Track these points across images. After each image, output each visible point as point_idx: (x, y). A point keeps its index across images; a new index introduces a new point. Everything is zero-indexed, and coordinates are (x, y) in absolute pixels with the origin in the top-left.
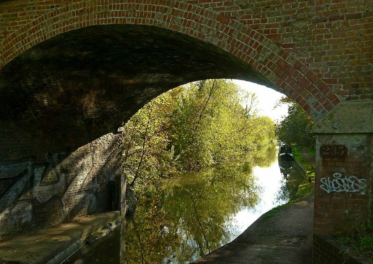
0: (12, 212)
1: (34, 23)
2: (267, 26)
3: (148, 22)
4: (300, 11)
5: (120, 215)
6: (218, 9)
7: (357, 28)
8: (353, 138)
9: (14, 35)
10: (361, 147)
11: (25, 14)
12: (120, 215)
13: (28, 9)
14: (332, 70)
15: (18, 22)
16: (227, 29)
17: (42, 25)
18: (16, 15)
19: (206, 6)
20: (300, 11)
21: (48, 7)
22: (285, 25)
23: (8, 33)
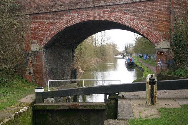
0: (49, 117)
1: (71, 18)
2: (143, 22)
3: (109, 19)
4: (151, 19)
5: (139, 104)
6: (130, 17)
7: (165, 23)
8: (165, 50)
9: (63, 22)
10: (167, 52)
11: (67, 15)
12: (139, 104)
13: (68, 14)
14: (159, 33)
15: (106, 10)
16: (132, 22)
17: (74, 19)
18: (64, 16)
19: (126, 16)
20: (151, 19)
21: (76, 14)
22: (147, 22)
23: (61, 21)
